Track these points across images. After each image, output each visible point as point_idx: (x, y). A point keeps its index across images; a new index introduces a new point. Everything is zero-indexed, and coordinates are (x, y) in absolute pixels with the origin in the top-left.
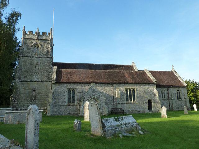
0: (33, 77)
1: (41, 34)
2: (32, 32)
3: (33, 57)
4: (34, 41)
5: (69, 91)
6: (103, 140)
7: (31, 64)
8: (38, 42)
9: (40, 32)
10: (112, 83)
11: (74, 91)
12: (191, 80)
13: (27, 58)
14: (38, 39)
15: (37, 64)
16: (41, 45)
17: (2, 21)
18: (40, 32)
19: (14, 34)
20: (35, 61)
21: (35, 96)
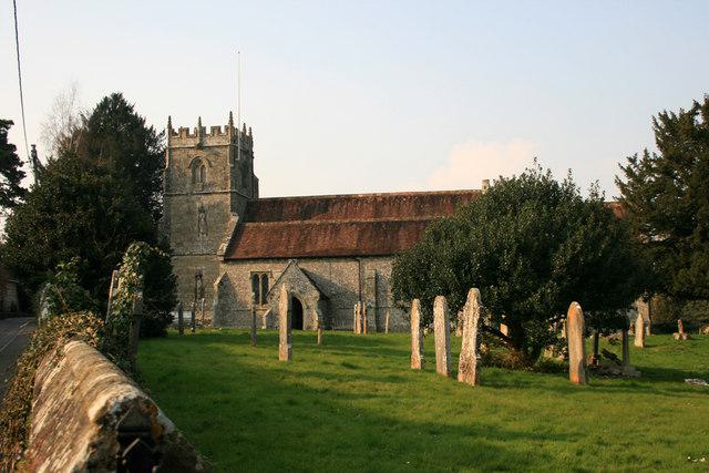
0: (196, 243)
1: (208, 131)
2: (188, 130)
3: (192, 194)
4: (192, 152)
5: (255, 278)
6: (505, 213)
7: (190, 213)
8: (202, 154)
9: (205, 128)
10: (357, 256)
11: (265, 278)
12: (139, 111)
13: (181, 197)
14: (200, 147)
15: (202, 210)
16: (210, 163)
17: (569, 193)
18: (205, 128)
19: (84, 133)
20: (198, 205)
21: (202, 289)
